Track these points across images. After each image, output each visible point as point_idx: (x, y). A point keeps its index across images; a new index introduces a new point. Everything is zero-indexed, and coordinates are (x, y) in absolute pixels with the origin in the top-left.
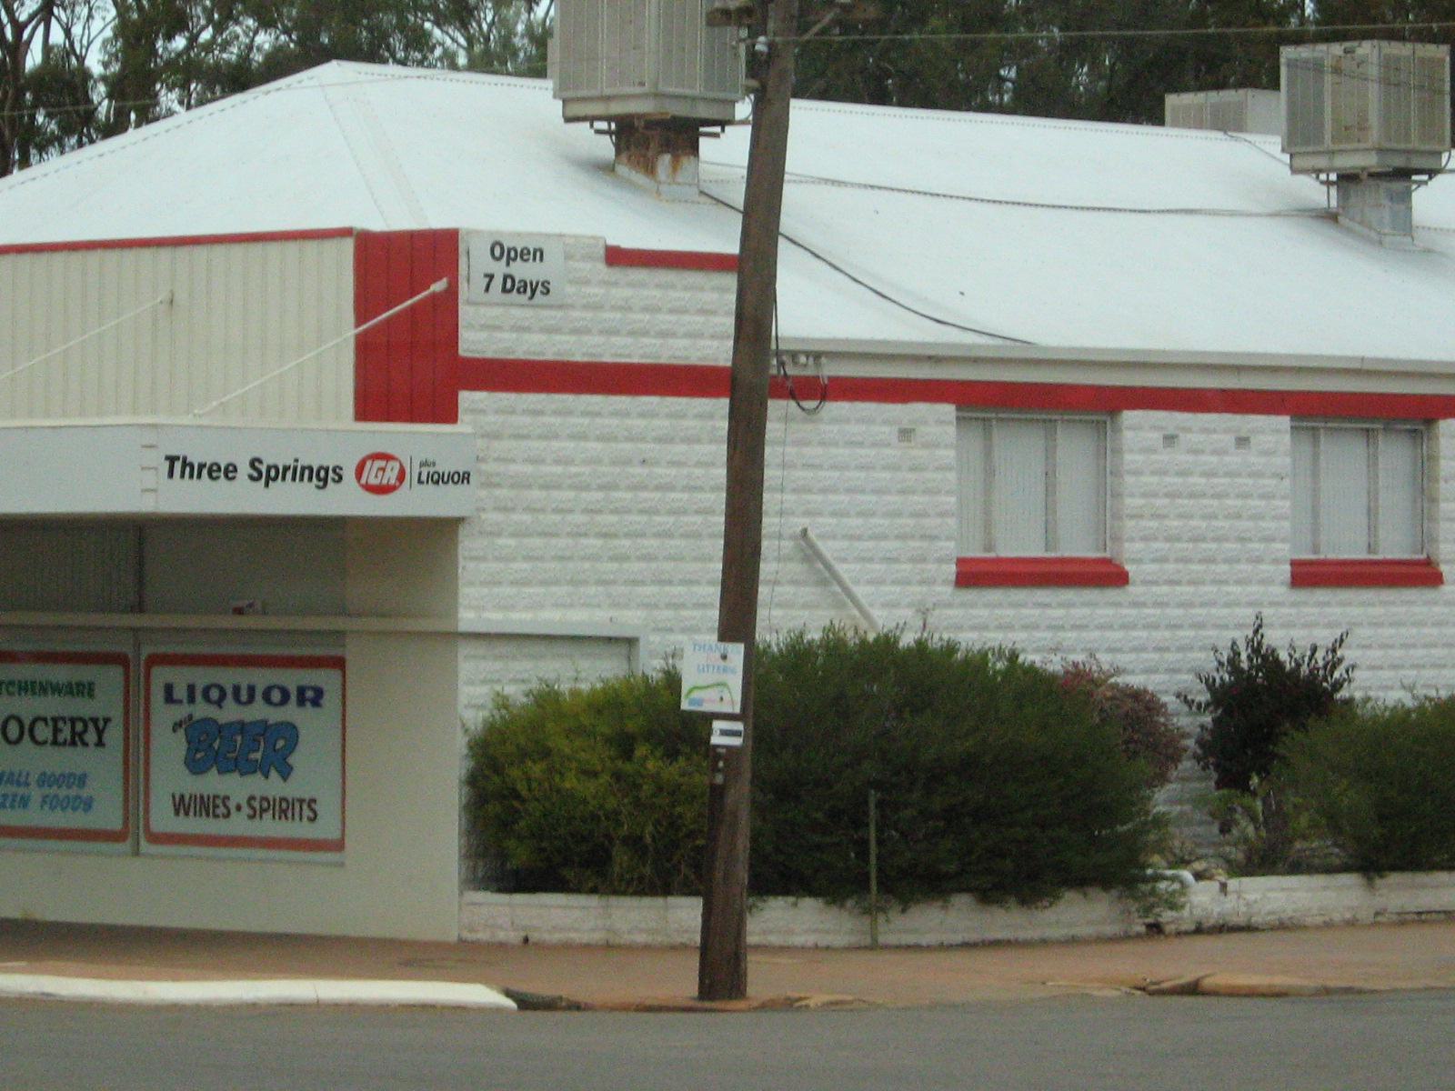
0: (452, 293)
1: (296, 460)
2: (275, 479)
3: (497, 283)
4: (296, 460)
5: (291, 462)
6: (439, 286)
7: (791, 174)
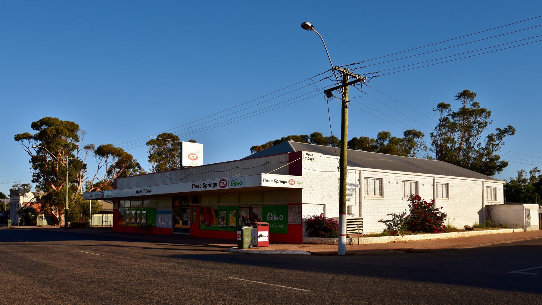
0: (301, 160)
1: (210, 183)
2: (207, 187)
3: (307, 158)
4: (210, 183)
5: (280, 180)
6: (299, 159)
7: (350, 185)
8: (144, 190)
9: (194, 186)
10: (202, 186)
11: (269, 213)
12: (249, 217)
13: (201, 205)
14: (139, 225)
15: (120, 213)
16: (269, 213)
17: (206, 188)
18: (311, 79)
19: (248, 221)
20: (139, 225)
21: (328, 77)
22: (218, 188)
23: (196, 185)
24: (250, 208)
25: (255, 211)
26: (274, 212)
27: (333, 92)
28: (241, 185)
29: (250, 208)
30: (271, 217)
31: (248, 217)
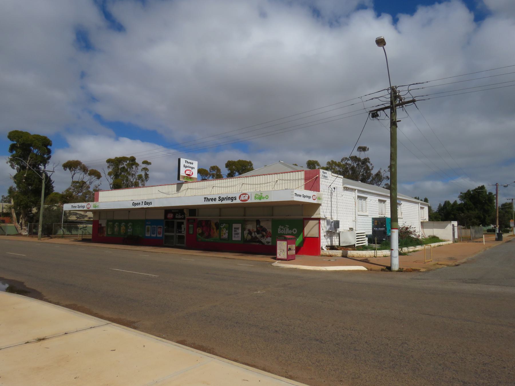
1: (227, 196)
2: (223, 200)
8: (142, 202)
9: (206, 199)
10: (77, 207)
11: (280, 227)
12: (256, 230)
13: (198, 218)
14: (331, 241)
15: (101, 225)
16: (280, 227)
17: (222, 202)
18: (360, 98)
19: (255, 234)
20: (331, 241)
21: (376, 98)
22: (238, 201)
23: (74, 206)
24: (258, 222)
25: (262, 224)
26: (287, 225)
27: (378, 113)
28: (266, 199)
29: (258, 222)
30: (282, 231)
31: (255, 230)
